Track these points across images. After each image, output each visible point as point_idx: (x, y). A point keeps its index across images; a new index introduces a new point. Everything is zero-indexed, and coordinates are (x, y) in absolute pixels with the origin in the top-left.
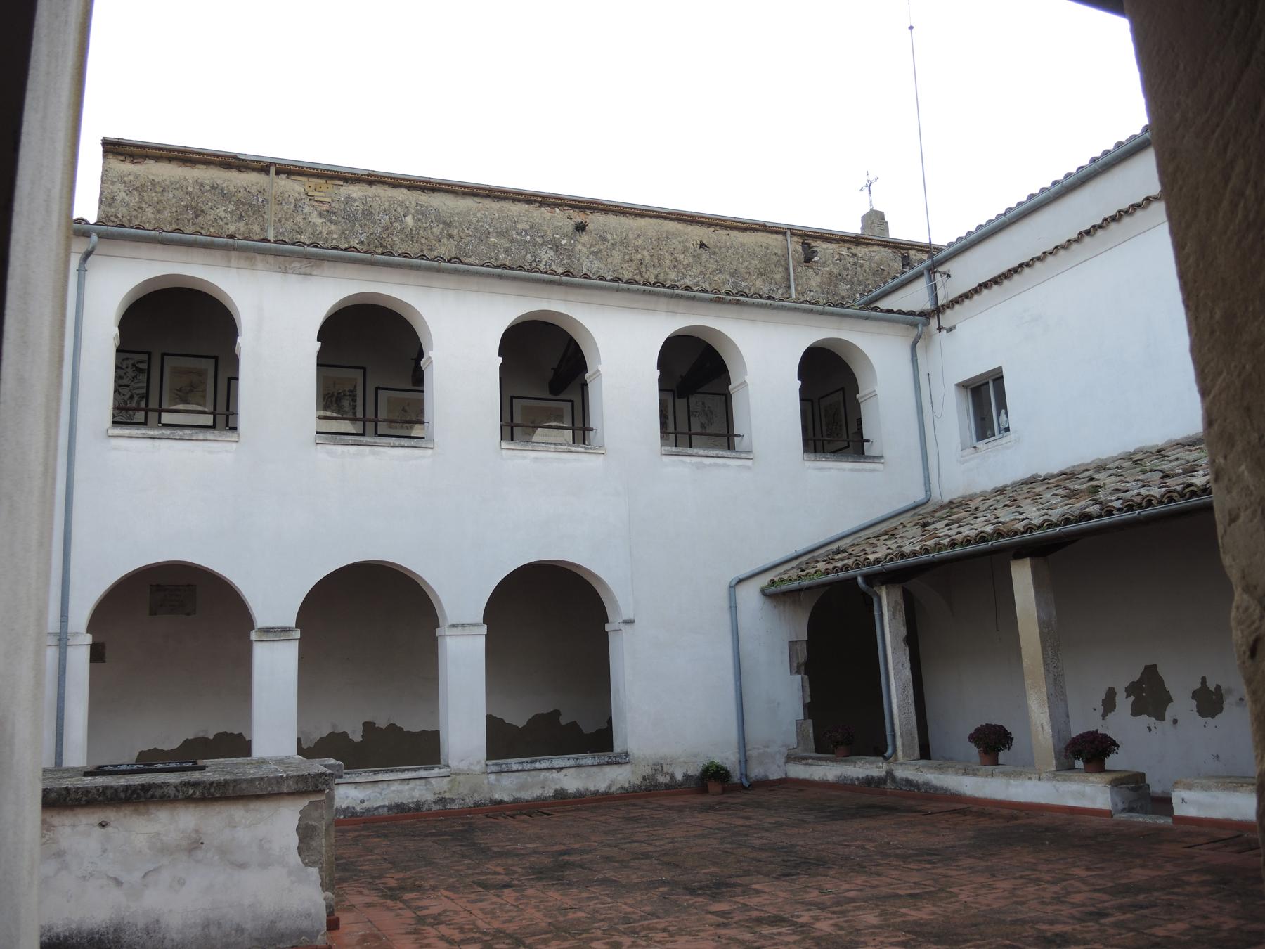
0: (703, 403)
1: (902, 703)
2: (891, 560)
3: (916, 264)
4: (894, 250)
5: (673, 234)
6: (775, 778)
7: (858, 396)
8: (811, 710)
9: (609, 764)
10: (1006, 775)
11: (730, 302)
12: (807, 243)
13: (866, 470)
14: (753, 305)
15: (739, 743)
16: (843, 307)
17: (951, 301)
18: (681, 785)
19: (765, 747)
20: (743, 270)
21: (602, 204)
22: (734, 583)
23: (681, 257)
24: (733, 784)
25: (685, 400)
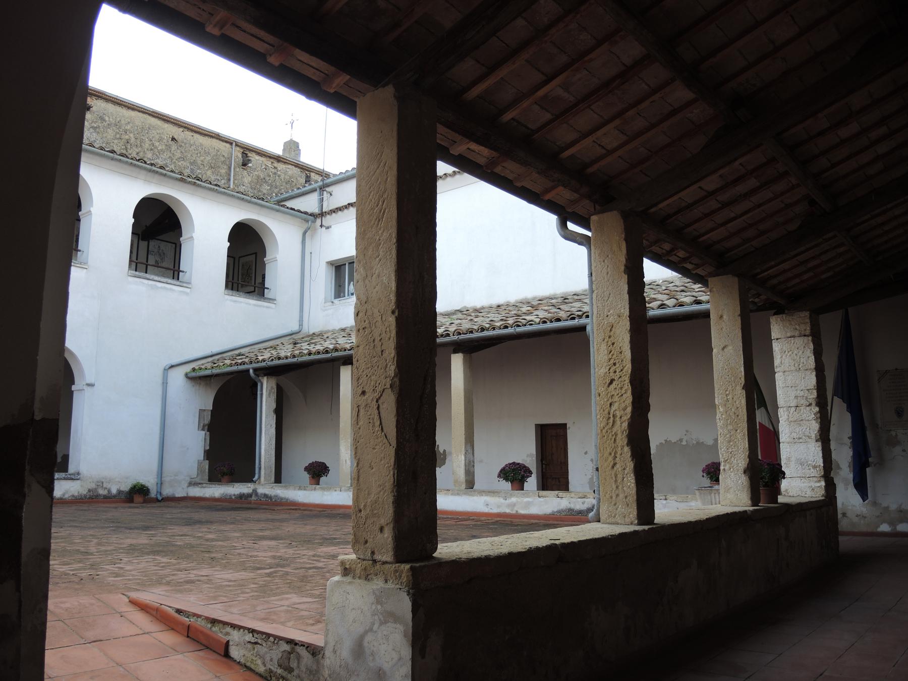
0: (159, 247)
1: (267, 448)
2: (272, 360)
3: (313, 183)
4: (302, 170)
5: (154, 127)
6: (180, 496)
7: (265, 259)
8: (208, 454)
9: (65, 479)
10: (323, 489)
11: (189, 183)
12: (245, 153)
13: (264, 307)
14: (205, 187)
15: (158, 472)
16: (263, 200)
17: (331, 210)
18: (115, 496)
19: (175, 476)
20: (199, 162)
21: (105, 95)
22: (167, 367)
23: (157, 144)
24: (151, 498)
25: (146, 243)
